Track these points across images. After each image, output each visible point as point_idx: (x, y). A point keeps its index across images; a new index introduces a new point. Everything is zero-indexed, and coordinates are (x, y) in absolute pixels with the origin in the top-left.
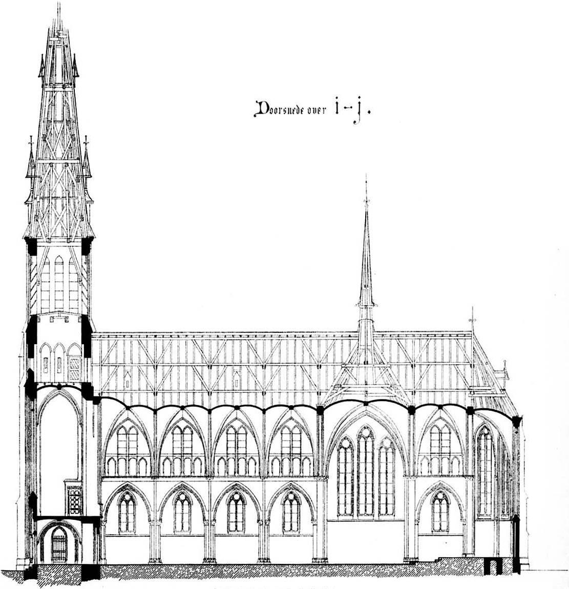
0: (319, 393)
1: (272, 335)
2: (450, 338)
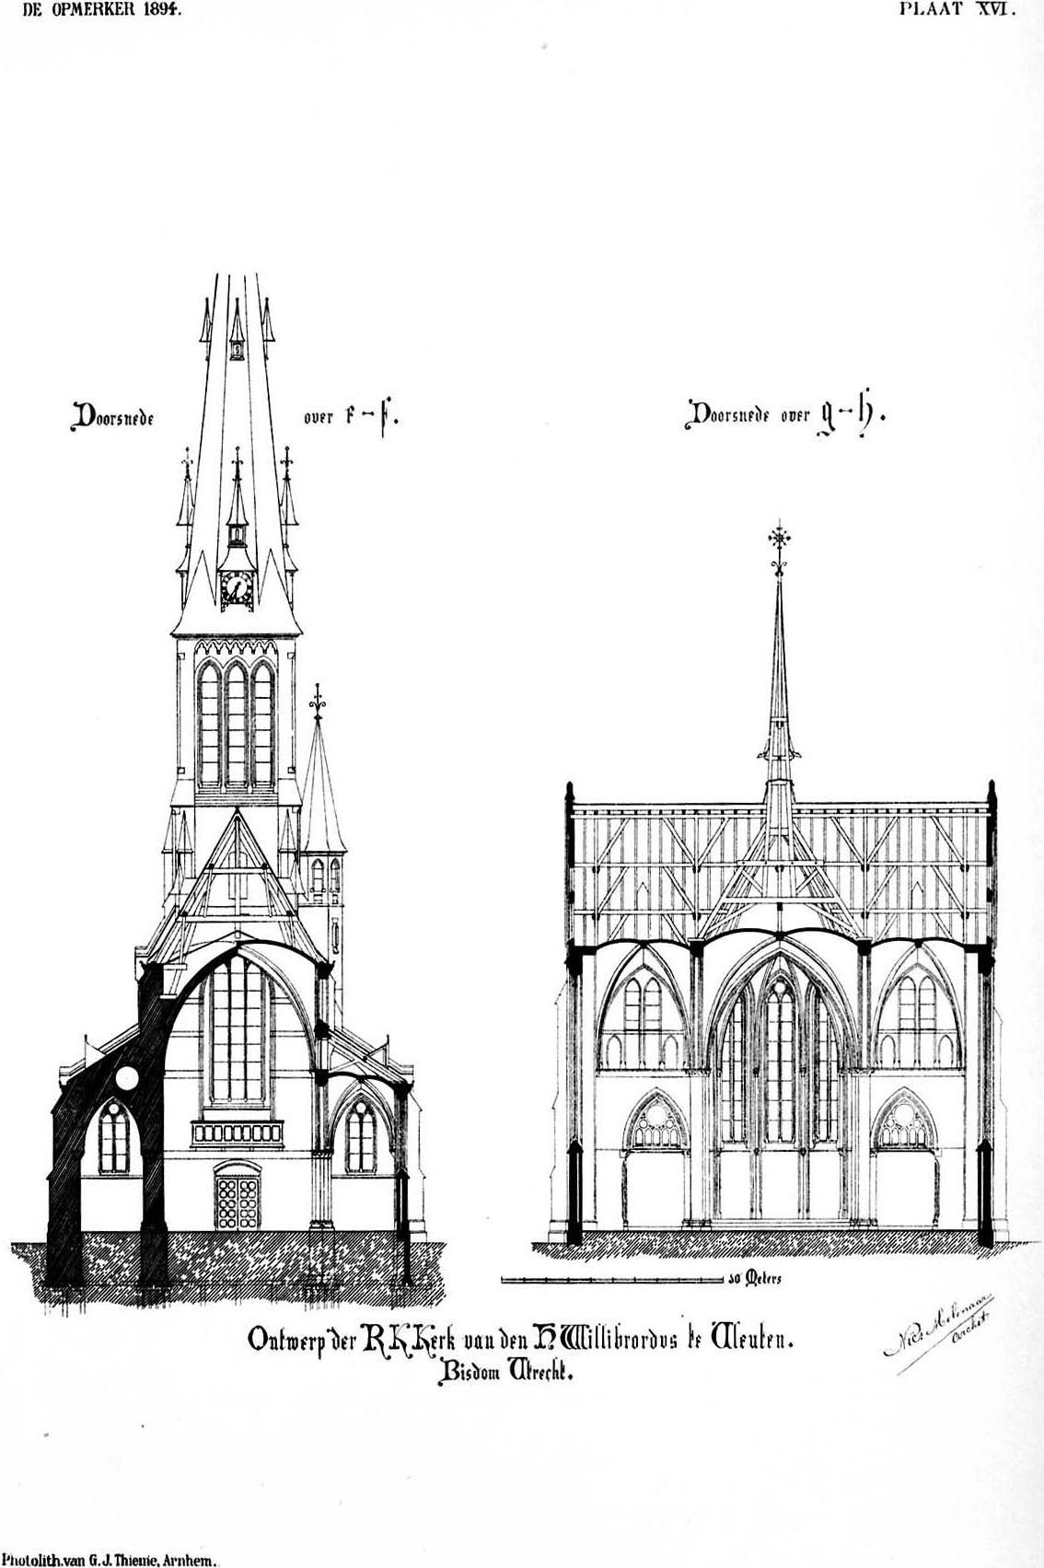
0: (697, 916)
1: (661, 811)
2: (924, 815)
